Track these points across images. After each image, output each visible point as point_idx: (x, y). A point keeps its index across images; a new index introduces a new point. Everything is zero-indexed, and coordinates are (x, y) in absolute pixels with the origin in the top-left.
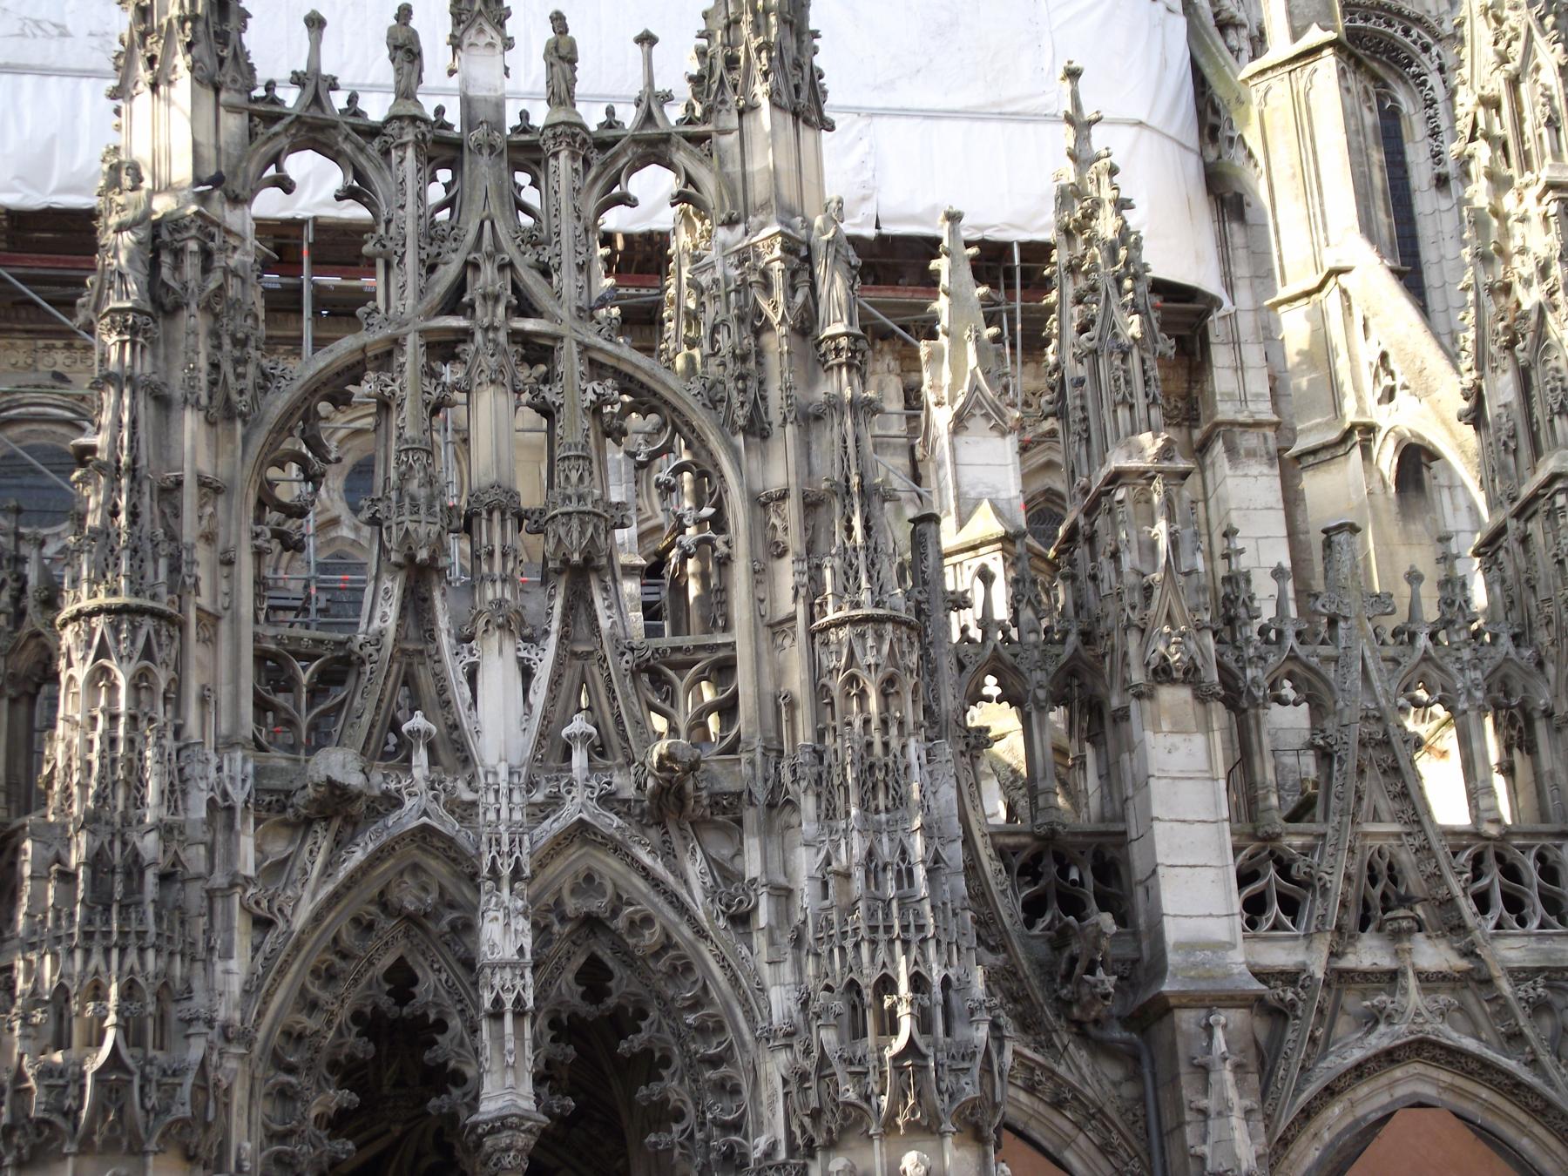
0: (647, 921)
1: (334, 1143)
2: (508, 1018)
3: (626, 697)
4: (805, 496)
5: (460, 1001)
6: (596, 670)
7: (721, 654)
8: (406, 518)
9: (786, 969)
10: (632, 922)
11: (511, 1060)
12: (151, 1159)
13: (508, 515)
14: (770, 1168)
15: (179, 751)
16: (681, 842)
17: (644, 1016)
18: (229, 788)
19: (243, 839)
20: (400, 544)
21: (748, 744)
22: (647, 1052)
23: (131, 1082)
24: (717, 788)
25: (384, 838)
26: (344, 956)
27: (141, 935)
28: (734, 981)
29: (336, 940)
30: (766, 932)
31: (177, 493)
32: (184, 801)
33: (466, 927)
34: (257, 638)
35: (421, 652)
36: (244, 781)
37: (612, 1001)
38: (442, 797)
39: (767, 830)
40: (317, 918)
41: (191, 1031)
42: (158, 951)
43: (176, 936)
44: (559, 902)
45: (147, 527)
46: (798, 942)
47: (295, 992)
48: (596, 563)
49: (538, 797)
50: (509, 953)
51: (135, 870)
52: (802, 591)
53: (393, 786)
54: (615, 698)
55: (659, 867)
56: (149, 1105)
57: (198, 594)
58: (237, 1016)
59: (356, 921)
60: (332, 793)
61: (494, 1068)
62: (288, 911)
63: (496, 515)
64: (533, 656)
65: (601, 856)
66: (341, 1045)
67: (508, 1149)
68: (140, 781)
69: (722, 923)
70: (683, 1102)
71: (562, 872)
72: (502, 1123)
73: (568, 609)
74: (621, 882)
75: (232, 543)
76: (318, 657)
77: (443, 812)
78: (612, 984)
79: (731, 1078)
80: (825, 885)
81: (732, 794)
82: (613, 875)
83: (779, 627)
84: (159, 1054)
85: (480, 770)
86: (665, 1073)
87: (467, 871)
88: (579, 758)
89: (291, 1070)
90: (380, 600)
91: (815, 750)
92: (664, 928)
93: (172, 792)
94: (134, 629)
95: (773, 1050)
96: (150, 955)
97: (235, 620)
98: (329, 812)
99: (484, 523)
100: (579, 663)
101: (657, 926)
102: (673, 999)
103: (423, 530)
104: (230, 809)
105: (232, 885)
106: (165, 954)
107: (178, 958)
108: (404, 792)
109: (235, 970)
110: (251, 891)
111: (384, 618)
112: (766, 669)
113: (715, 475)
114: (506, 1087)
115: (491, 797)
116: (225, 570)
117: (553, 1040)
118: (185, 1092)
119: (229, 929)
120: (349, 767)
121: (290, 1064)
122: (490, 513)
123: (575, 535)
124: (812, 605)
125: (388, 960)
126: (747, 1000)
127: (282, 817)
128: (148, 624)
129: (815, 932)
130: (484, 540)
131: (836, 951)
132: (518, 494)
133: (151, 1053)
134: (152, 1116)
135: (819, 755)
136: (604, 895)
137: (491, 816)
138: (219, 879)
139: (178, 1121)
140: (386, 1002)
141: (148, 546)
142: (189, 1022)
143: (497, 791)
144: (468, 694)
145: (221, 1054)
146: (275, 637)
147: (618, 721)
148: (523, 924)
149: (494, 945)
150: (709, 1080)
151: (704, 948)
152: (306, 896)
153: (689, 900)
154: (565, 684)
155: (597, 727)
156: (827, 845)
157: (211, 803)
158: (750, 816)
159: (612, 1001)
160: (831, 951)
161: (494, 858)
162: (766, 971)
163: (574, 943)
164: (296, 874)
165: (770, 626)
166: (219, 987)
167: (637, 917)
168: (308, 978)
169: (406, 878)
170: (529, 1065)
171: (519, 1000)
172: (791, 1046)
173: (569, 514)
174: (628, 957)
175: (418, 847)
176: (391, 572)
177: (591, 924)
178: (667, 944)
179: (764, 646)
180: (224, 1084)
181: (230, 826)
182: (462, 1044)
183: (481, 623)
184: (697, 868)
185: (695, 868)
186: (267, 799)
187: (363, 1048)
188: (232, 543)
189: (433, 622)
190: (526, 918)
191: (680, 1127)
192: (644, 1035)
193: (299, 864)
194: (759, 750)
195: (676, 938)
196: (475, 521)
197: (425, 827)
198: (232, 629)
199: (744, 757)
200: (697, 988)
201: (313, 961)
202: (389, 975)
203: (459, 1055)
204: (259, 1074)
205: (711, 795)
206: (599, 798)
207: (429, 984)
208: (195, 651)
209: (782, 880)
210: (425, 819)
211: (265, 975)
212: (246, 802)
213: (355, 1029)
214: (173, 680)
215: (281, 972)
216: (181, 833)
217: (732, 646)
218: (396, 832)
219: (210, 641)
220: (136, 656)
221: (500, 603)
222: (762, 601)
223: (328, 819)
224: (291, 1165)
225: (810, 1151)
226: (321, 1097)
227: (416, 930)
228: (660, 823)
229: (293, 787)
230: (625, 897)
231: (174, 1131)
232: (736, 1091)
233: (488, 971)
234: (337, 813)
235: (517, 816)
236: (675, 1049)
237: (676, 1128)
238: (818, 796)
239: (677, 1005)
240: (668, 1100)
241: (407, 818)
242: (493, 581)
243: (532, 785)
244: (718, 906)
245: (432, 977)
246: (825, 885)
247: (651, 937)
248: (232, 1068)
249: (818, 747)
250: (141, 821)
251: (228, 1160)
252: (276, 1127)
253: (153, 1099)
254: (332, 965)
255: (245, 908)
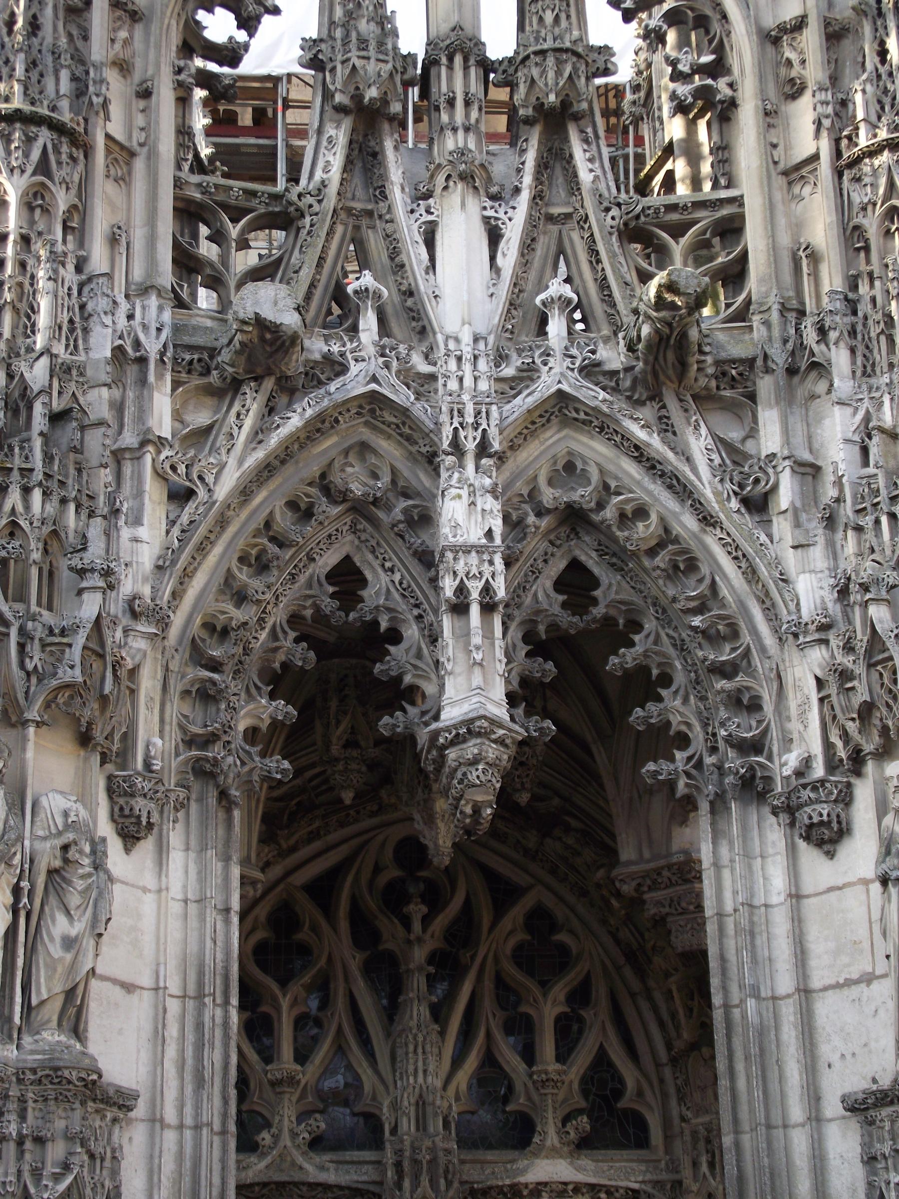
0: (641, 512)
1: (267, 761)
2: (475, 610)
3: (612, 256)
4: (827, 23)
5: (417, 606)
6: (575, 236)
7: (725, 211)
8: (354, 54)
9: (818, 555)
10: (622, 516)
11: (478, 657)
12: (32, 730)
13: (472, 61)
14: (804, 786)
15: (81, 286)
16: (681, 413)
17: (637, 627)
18: (142, 337)
19: (156, 395)
20: (346, 83)
21: (761, 304)
22: (643, 670)
23: (8, 635)
24: (723, 355)
25: (326, 403)
26: (280, 542)
27: (26, 472)
28: (751, 574)
29: (268, 525)
30: (789, 515)
31: (85, 14)
32: (85, 340)
33: (424, 518)
34: (178, 183)
35: (370, 214)
36: (159, 330)
37: (598, 611)
38: (395, 364)
39: (786, 399)
40: (245, 492)
41: (84, 584)
42: (46, 494)
43: (70, 482)
44: (533, 495)
45: (49, 40)
46: (830, 522)
47: (220, 579)
48: (575, 108)
49: (509, 371)
50: (475, 536)
51: (22, 405)
52: (827, 123)
53: (336, 348)
54: (599, 261)
55: (655, 442)
56: (30, 666)
57: (107, 118)
58: (147, 591)
59: (292, 505)
60: (262, 339)
61: (458, 670)
62: (210, 479)
63: (458, 59)
64: (501, 215)
65: (585, 439)
66: (276, 650)
67: (474, 762)
68: (32, 308)
69: (734, 504)
70: (688, 725)
71: (537, 458)
72: (469, 729)
73: (542, 167)
74: (611, 468)
75: (150, 72)
76: (251, 211)
77: (394, 380)
78: (597, 593)
79: (748, 689)
80: (865, 451)
81: (742, 361)
82: (600, 460)
83: (797, 173)
84: (45, 613)
85: (440, 338)
86: (664, 693)
87: (424, 450)
88: (556, 327)
89: (215, 666)
90: (323, 150)
91: (846, 299)
92: (662, 519)
93: (72, 330)
94: (29, 140)
95: (801, 648)
96: (37, 496)
97: (153, 156)
98: (259, 371)
99: (444, 70)
100: (554, 229)
101: (654, 517)
102: (674, 600)
103: (372, 67)
104: (142, 361)
105: (143, 443)
106: (55, 498)
107: (72, 507)
108: (349, 356)
109: (144, 541)
110: (166, 453)
111: (326, 170)
112: (782, 221)
113: (715, 17)
114: (471, 685)
115: (453, 365)
116: (142, 104)
117: (528, 655)
118: (76, 653)
119: (139, 494)
120: (281, 304)
121: (212, 659)
122: (451, 59)
123: (551, 74)
124: (837, 141)
125: (329, 559)
126: (767, 594)
127: (205, 380)
128: (44, 136)
129: (854, 504)
130: (444, 89)
131: (884, 520)
132: (484, 44)
133: (34, 608)
134: (34, 680)
135: (852, 306)
136: (589, 483)
137: (453, 385)
138: (129, 439)
139: (67, 686)
140: (328, 605)
141: (49, 59)
142: (81, 572)
143: (459, 359)
144: (425, 256)
145: (126, 631)
146: (199, 185)
147: (603, 284)
148: (491, 504)
149: (457, 526)
150: (723, 690)
151: (711, 541)
152: (232, 462)
153: (693, 477)
154: (539, 252)
155: (578, 295)
156: (866, 404)
157: (118, 351)
158: (765, 385)
159: (598, 611)
160: (877, 522)
161: (456, 429)
162: (791, 559)
163: (551, 542)
164: (222, 440)
165: (785, 173)
166: (125, 557)
167: (629, 508)
168: (234, 563)
169: (351, 458)
170: (501, 668)
171: (487, 589)
172: (826, 642)
173: (542, 53)
174: (618, 557)
175: (367, 424)
176: (337, 116)
177: (574, 518)
178: (666, 537)
179: (778, 196)
180: (129, 663)
181: (143, 381)
182: (419, 655)
183: (440, 180)
184: (702, 443)
185: (699, 444)
186: (188, 357)
187: (303, 656)
188: (150, 72)
189: (384, 177)
190: (496, 498)
191: (686, 754)
192: (639, 649)
193: (225, 430)
194: (776, 307)
195: (677, 529)
196: (433, 71)
197: (374, 392)
198: (148, 166)
199: (756, 320)
200: (703, 587)
201: (241, 543)
202: (333, 576)
203: (415, 667)
204: (174, 666)
205: (717, 363)
206: (581, 370)
207: (379, 586)
208: (103, 189)
209: (806, 456)
210: (373, 386)
211: (181, 549)
212: (162, 354)
213: (292, 635)
214: (75, 207)
215: (202, 549)
216: (81, 374)
217: (738, 201)
218: (339, 397)
219: (124, 180)
220: (30, 170)
221: (462, 152)
222: (775, 146)
223: (258, 379)
224: (212, 776)
225: (857, 760)
226: (251, 706)
227: (363, 524)
228: (655, 396)
229: (218, 344)
230: (613, 484)
231: (61, 700)
232: (755, 706)
233: (449, 555)
234: (269, 373)
235: (483, 386)
236: (678, 664)
237: (679, 755)
238: (853, 351)
239: (678, 606)
240: (668, 724)
241: (355, 382)
242: (455, 130)
243: (500, 358)
244: (728, 485)
245: (384, 578)
246: (865, 451)
247: (644, 531)
248: (136, 645)
249: (851, 295)
250: (30, 350)
251: (134, 756)
252: (197, 730)
253: (36, 658)
254: (264, 551)
255: (159, 474)
